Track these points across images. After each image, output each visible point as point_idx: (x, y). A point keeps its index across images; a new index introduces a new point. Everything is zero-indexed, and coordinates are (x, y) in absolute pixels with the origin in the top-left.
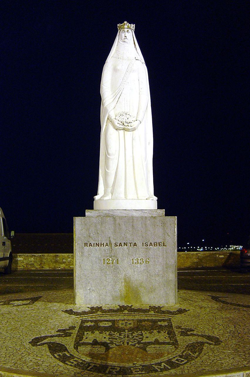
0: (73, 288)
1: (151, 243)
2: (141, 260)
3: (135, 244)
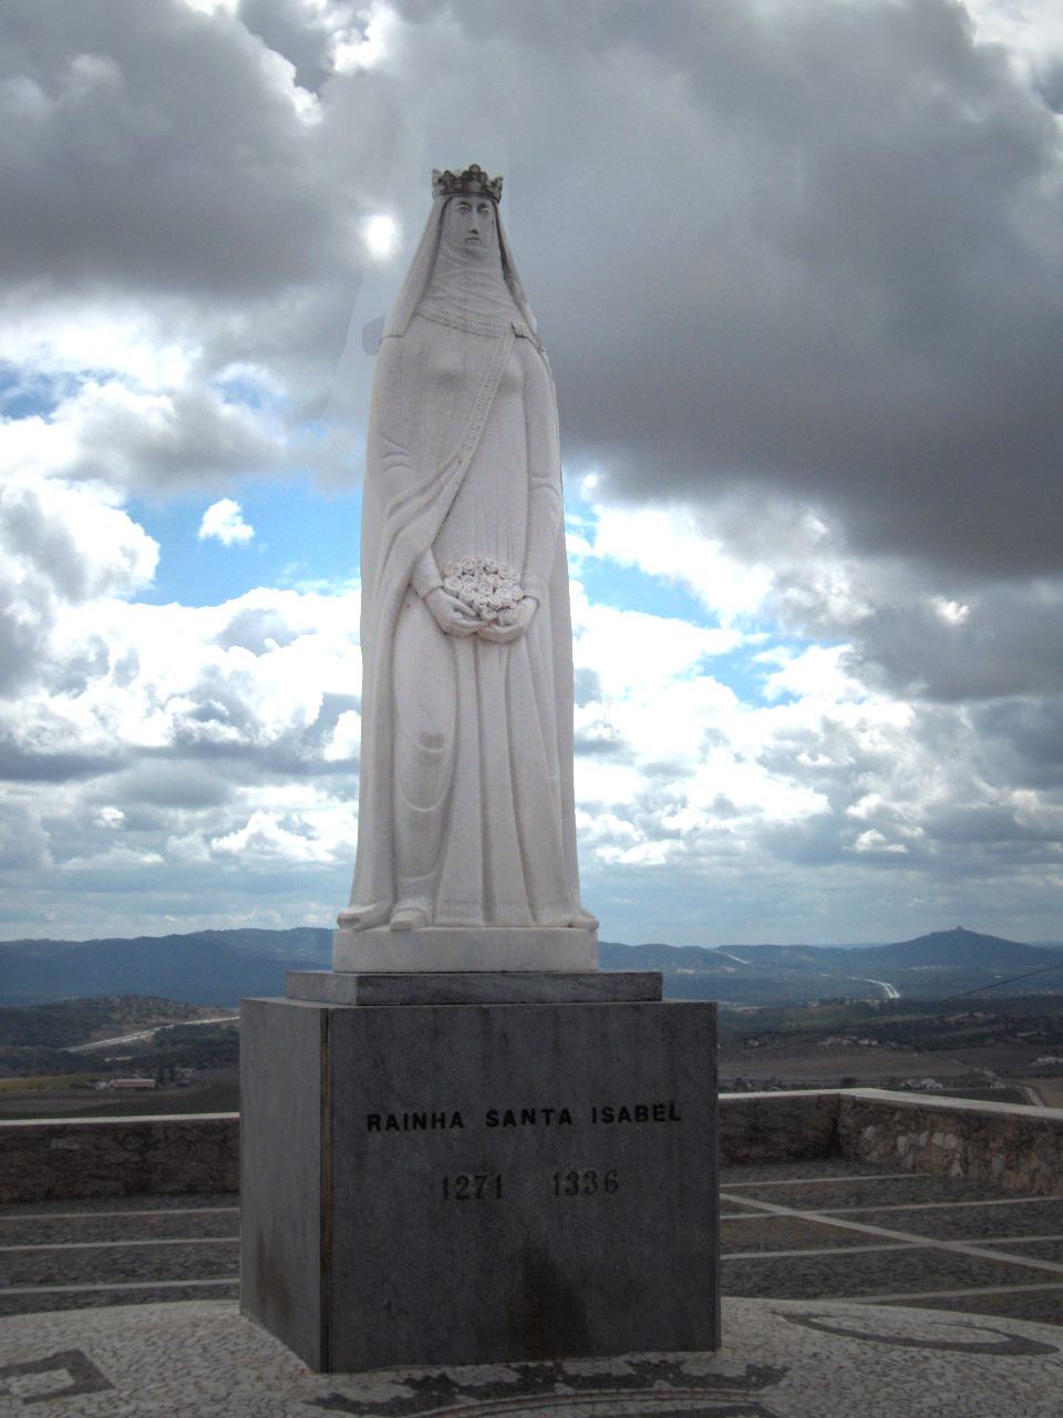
0: (322, 1372)
1: (624, 1110)
2: (586, 1176)
3: (565, 1117)
